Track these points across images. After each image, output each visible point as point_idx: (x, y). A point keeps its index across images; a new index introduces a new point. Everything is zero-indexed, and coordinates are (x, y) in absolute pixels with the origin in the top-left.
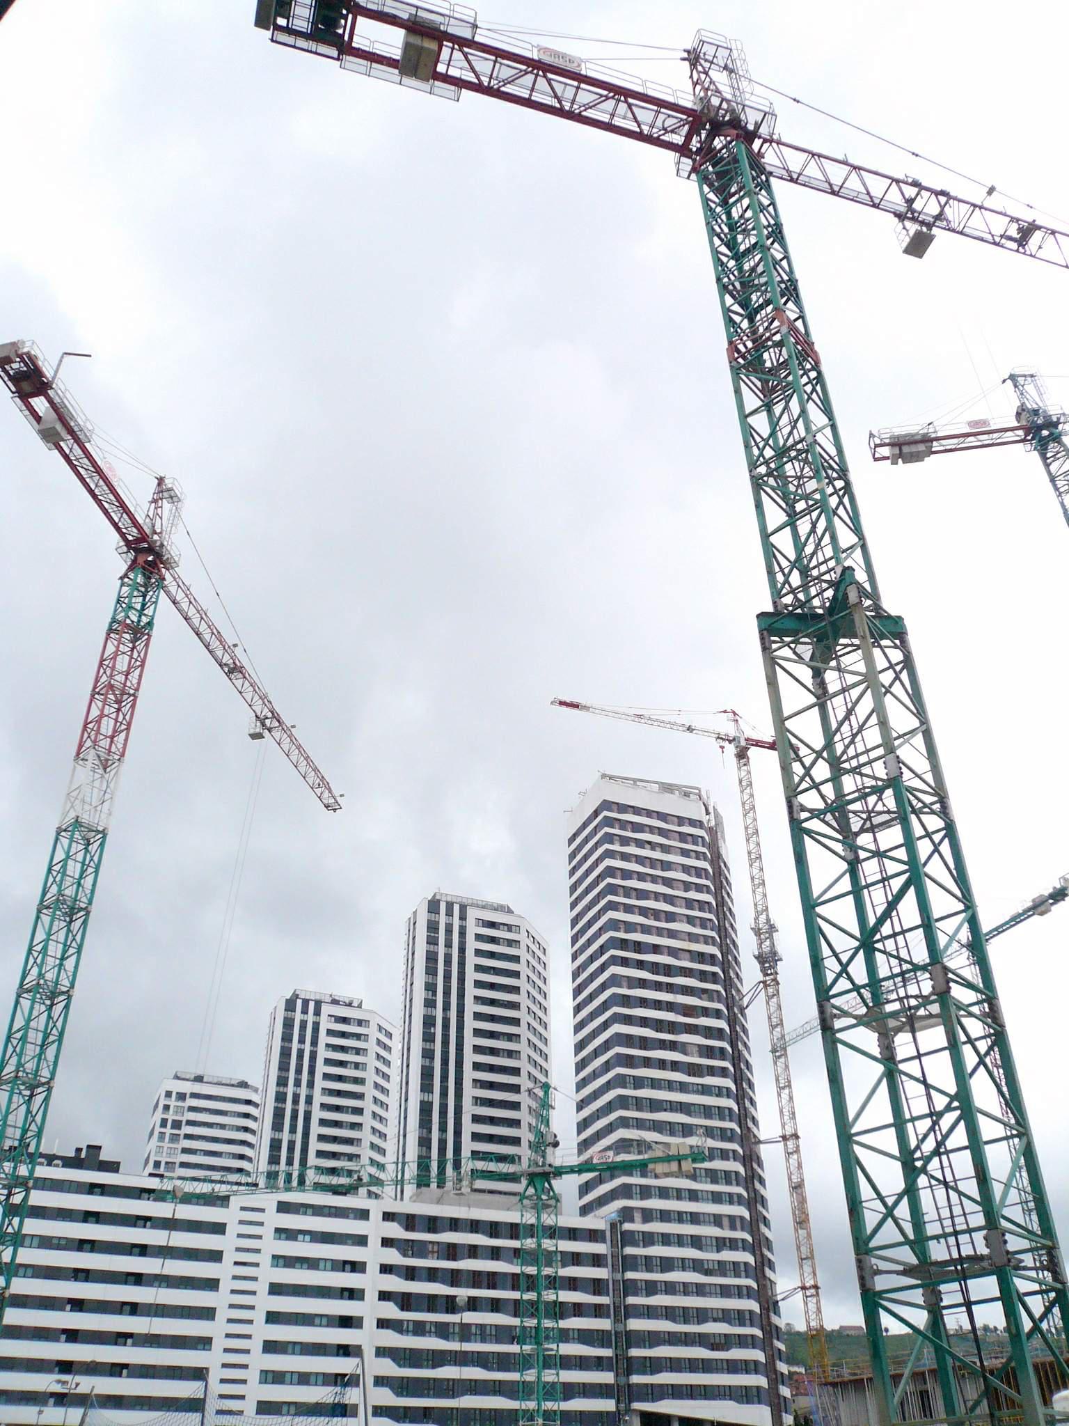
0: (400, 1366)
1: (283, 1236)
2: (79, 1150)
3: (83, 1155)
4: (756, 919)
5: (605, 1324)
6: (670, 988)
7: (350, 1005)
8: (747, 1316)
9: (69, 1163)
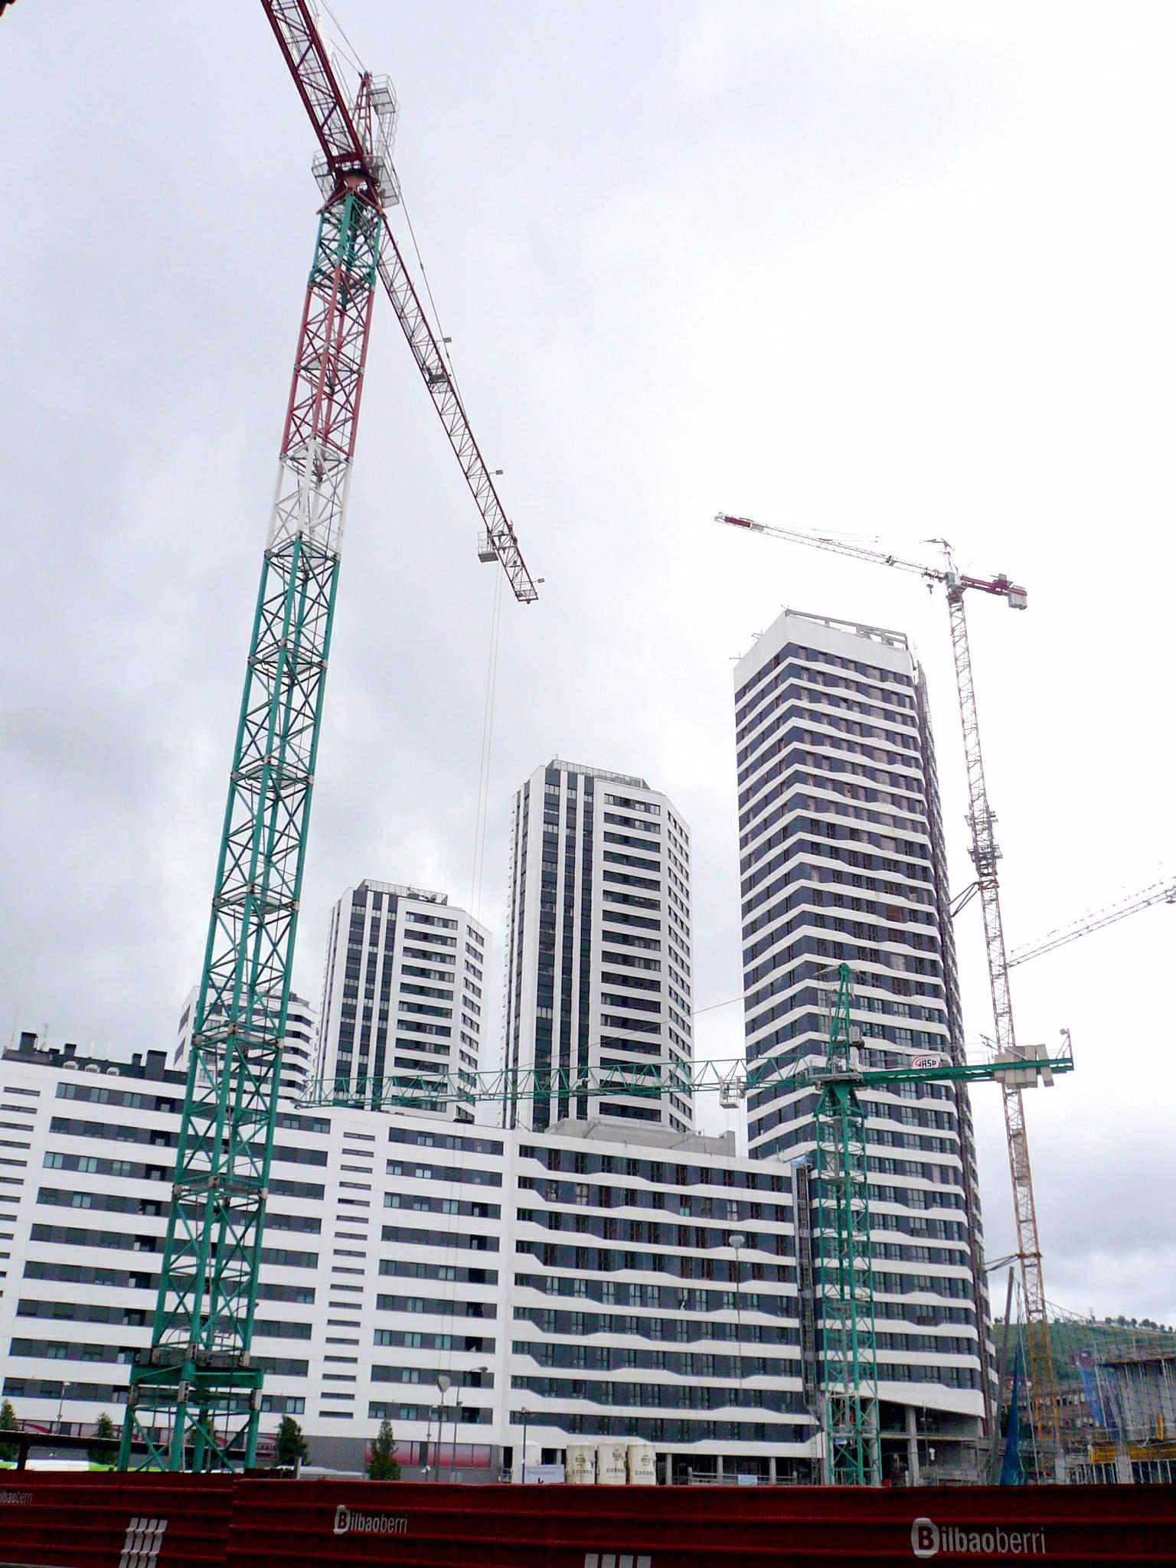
0: (543, 1330)
1: (398, 1170)
2: (137, 1057)
3: (143, 1063)
4: (971, 806)
5: (790, 1289)
6: (872, 884)
7: (432, 901)
8: (960, 1286)
9: (127, 1071)
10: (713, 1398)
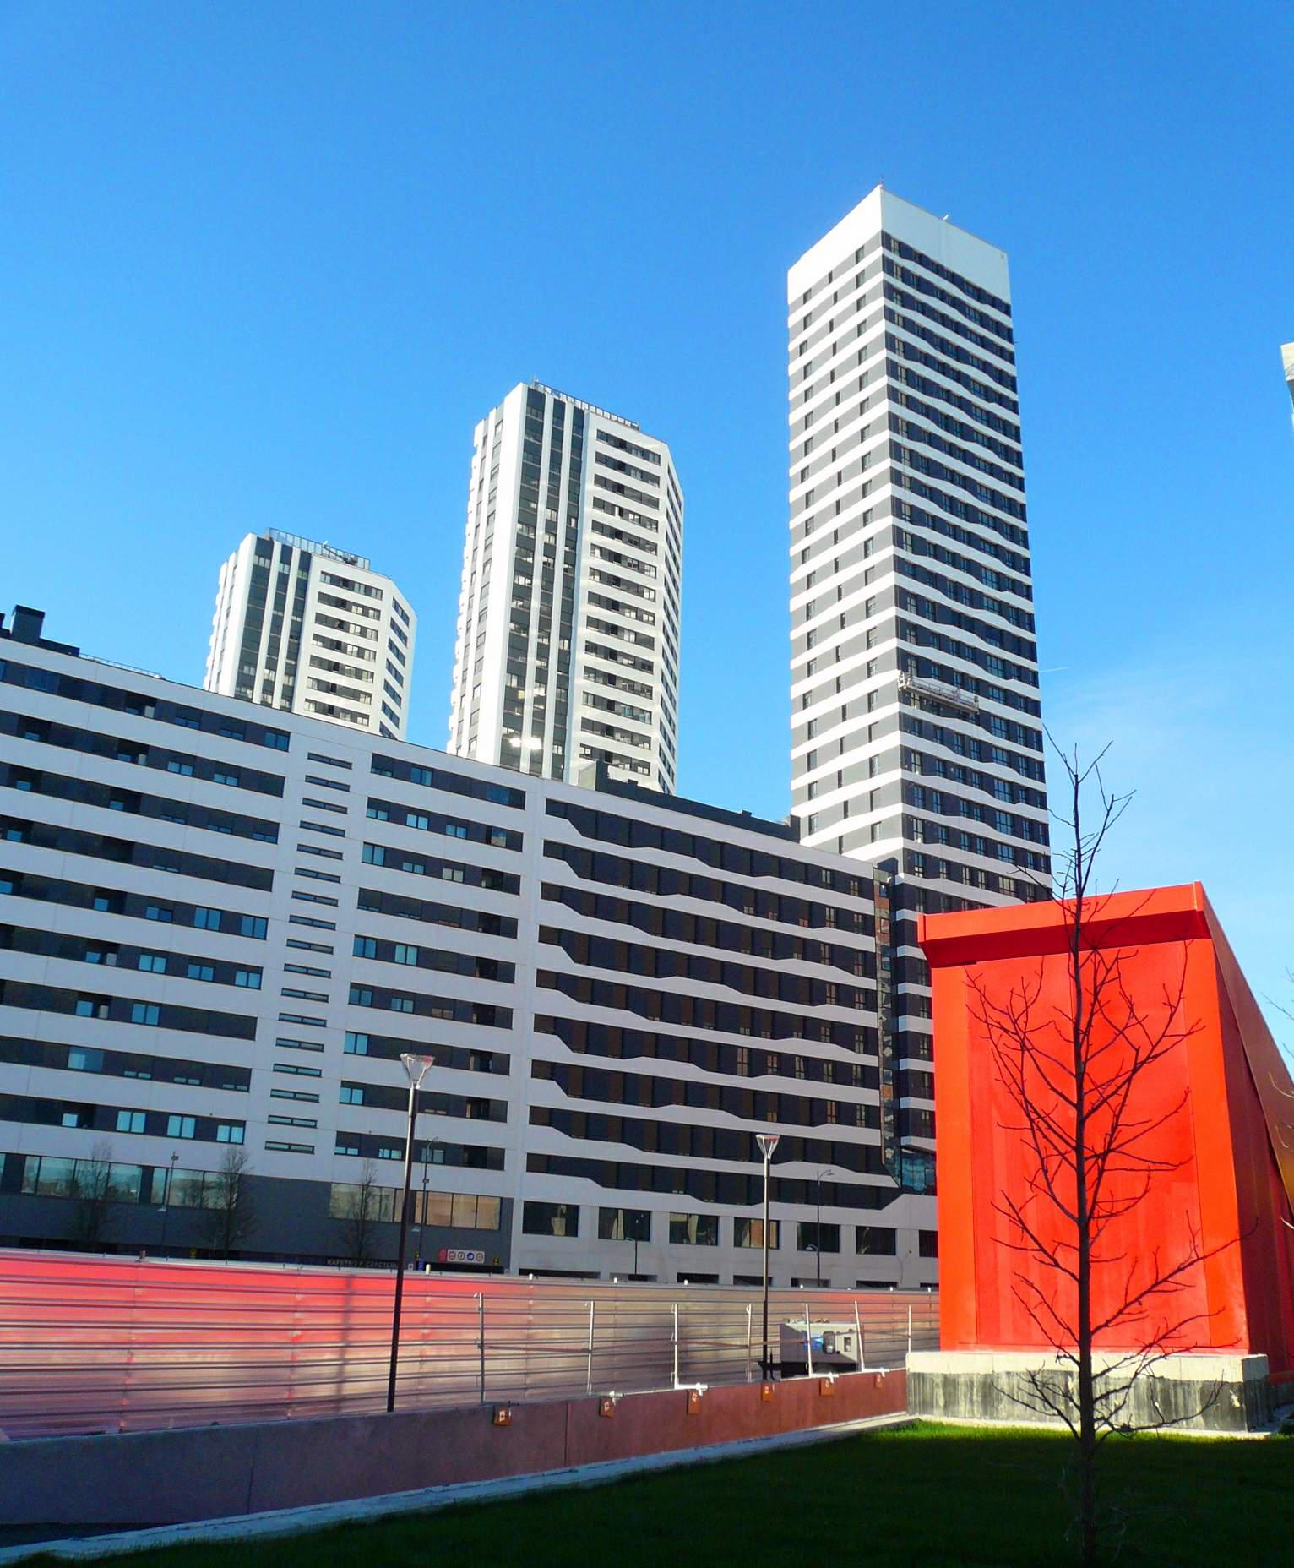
10: (780, 1026)
